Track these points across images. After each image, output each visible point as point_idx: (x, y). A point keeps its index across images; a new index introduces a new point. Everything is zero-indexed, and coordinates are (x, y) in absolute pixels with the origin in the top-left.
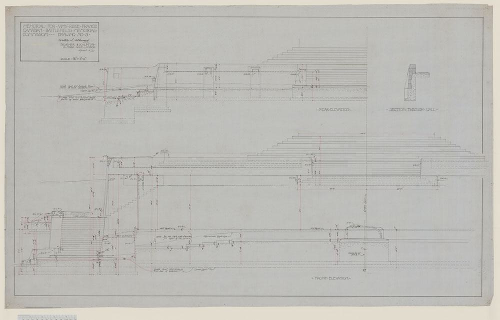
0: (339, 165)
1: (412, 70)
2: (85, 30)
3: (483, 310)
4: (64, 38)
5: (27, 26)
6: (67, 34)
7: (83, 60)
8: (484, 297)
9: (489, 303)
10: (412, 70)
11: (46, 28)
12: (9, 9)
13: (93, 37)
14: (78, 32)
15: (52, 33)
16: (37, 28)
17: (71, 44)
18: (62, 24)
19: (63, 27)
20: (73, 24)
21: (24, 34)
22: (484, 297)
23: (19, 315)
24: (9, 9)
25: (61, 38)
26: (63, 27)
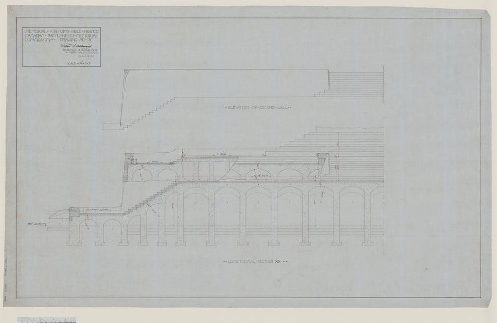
0: (363, 153)
1: (131, 161)
2: (87, 36)
3: (480, 311)
4: (67, 43)
5: (29, 31)
6: (69, 39)
7: (88, 65)
8: (482, 299)
9: (487, 304)
10: (131, 161)
11: (49, 33)
12: (10, 8)
13: (95, 43)
14: (78, 36)
15: (54, 38)
16: (39, 34)
17: (73, 50)
18: (64, 29)
19: (65, 33)
20: (75, 29)
21: (26, 40)
22: (482, 299)
23: (18, 318)
24: (10, 8)
25: (63, 43)
26: (65, 33)
